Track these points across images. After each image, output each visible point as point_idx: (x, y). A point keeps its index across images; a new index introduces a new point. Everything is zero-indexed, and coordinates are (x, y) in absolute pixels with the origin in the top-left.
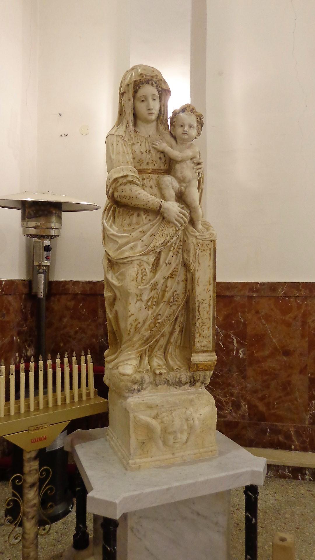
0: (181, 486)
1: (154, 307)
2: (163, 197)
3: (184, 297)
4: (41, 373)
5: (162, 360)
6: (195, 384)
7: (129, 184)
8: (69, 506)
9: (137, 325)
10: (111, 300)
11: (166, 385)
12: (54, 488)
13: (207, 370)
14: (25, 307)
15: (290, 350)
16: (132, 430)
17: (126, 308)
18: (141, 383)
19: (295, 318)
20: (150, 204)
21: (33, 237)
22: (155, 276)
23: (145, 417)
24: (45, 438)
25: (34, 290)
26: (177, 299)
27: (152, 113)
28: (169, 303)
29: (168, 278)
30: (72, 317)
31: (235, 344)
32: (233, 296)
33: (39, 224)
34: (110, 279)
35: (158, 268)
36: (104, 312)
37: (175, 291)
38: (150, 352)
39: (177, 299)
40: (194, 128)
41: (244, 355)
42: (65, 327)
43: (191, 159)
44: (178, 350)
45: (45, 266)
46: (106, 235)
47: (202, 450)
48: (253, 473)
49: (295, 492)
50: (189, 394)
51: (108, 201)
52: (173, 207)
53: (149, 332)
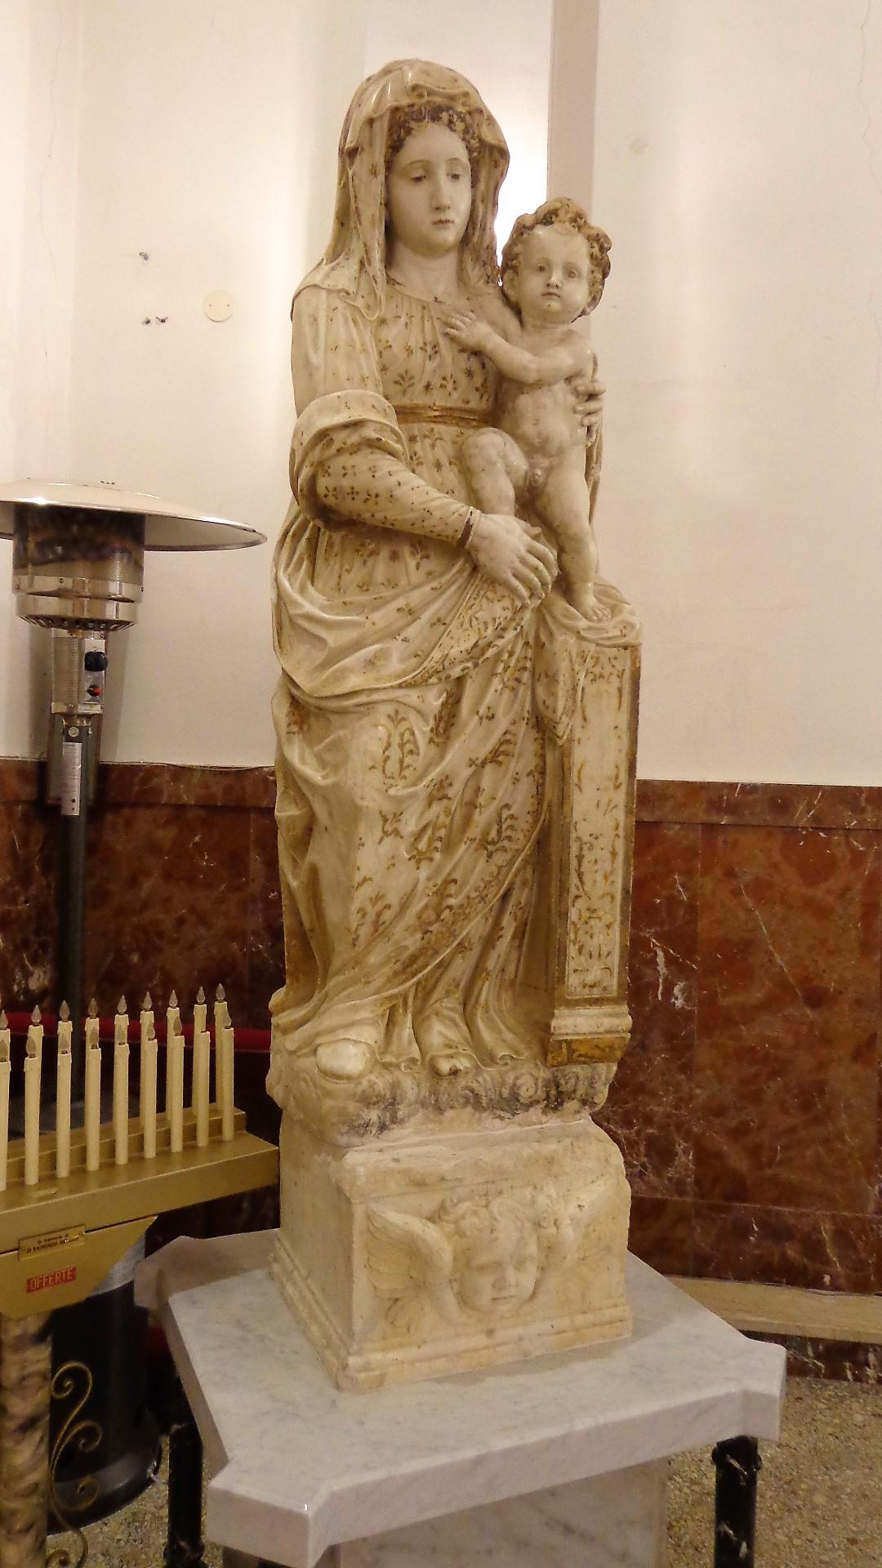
0: (517, 1449)
1: (437, 856)
2: (475, 499)
3: (536, 822)
4: (65, 1062)
5: (456, 1025)
6: (561, 1104)
7: (368, 451)
8: (147, 1464)
9: (379, 915)
10: (298, 831)
11: (469, 1109)
12: (100, 1431)
13: (601, 1060)
14: (25, 841)
15: (827, 990)
16: (358, 1259)
17: (347, 861)
18: (391, 1103)
19: (842, 895)
20: (434, 520)
21: (49, 626)
22: (442, 757)
23: (402, 1218)
24: (72, 1275)
25: (53, 792)
26: (509, 833)
27: (447, 221)
28: (484, 843)
29: (484, 764)
30: (167, 877)
31: (662, 968)
32: (657, 824)
33: (68, 583)
34: (296, 761)
35: (453, 731)
36: (272, 863)
37: (507, 806)
38: (418, 1002)
39: (509, 833)
40: (580, 276)
41: (687, 999)
42: (146, 905)
43: (568, 380)
44: (507, 996)
45: (88, 717)
46: (285, 621)
47: (580, 1319)
48: (749, 1399)
49: (837, 1421)
50: (542, 1137)
51: (296, 508)
52: (506, 534)
53: (419, 936)
